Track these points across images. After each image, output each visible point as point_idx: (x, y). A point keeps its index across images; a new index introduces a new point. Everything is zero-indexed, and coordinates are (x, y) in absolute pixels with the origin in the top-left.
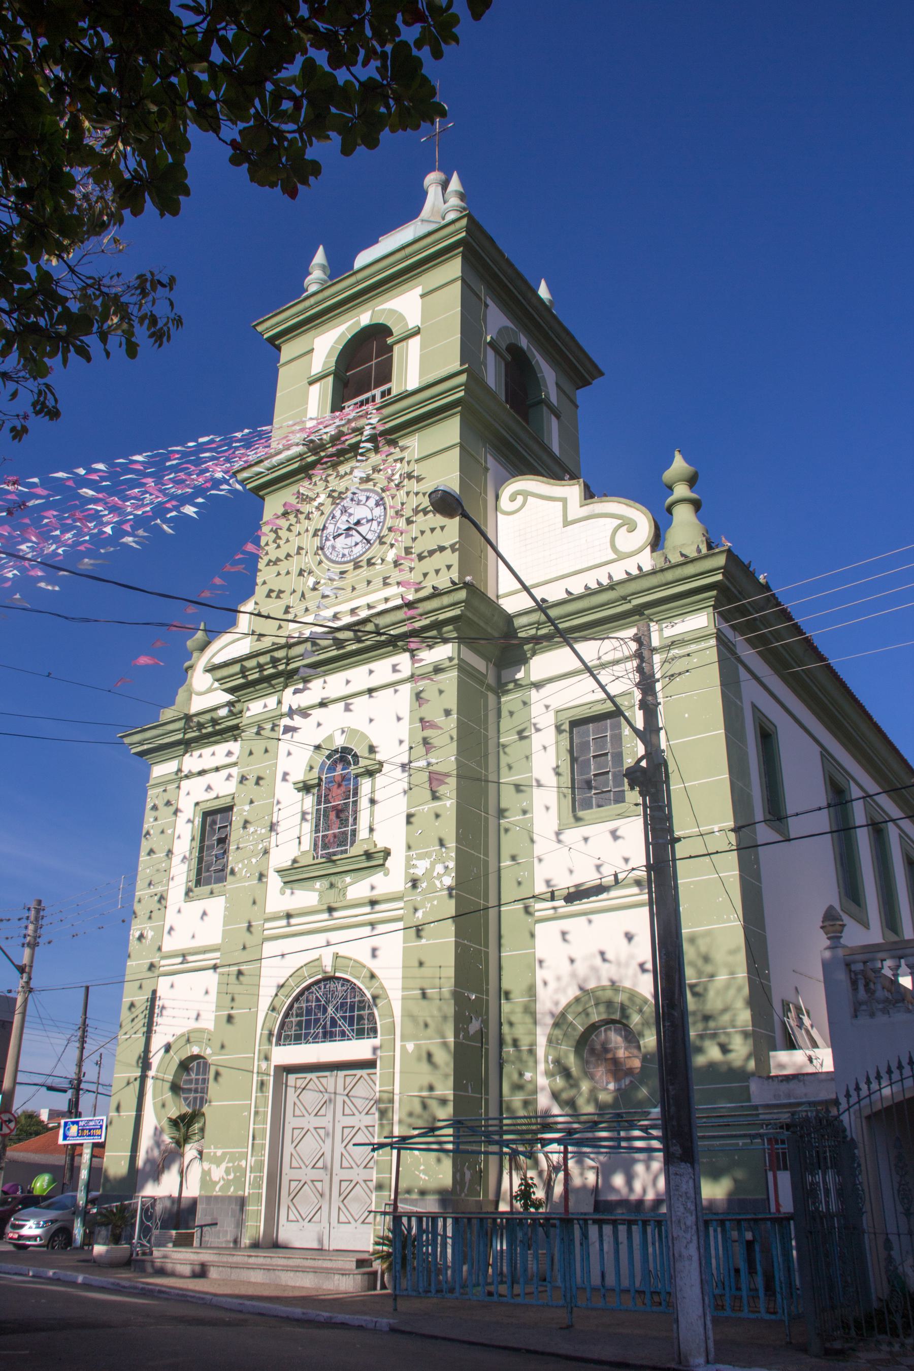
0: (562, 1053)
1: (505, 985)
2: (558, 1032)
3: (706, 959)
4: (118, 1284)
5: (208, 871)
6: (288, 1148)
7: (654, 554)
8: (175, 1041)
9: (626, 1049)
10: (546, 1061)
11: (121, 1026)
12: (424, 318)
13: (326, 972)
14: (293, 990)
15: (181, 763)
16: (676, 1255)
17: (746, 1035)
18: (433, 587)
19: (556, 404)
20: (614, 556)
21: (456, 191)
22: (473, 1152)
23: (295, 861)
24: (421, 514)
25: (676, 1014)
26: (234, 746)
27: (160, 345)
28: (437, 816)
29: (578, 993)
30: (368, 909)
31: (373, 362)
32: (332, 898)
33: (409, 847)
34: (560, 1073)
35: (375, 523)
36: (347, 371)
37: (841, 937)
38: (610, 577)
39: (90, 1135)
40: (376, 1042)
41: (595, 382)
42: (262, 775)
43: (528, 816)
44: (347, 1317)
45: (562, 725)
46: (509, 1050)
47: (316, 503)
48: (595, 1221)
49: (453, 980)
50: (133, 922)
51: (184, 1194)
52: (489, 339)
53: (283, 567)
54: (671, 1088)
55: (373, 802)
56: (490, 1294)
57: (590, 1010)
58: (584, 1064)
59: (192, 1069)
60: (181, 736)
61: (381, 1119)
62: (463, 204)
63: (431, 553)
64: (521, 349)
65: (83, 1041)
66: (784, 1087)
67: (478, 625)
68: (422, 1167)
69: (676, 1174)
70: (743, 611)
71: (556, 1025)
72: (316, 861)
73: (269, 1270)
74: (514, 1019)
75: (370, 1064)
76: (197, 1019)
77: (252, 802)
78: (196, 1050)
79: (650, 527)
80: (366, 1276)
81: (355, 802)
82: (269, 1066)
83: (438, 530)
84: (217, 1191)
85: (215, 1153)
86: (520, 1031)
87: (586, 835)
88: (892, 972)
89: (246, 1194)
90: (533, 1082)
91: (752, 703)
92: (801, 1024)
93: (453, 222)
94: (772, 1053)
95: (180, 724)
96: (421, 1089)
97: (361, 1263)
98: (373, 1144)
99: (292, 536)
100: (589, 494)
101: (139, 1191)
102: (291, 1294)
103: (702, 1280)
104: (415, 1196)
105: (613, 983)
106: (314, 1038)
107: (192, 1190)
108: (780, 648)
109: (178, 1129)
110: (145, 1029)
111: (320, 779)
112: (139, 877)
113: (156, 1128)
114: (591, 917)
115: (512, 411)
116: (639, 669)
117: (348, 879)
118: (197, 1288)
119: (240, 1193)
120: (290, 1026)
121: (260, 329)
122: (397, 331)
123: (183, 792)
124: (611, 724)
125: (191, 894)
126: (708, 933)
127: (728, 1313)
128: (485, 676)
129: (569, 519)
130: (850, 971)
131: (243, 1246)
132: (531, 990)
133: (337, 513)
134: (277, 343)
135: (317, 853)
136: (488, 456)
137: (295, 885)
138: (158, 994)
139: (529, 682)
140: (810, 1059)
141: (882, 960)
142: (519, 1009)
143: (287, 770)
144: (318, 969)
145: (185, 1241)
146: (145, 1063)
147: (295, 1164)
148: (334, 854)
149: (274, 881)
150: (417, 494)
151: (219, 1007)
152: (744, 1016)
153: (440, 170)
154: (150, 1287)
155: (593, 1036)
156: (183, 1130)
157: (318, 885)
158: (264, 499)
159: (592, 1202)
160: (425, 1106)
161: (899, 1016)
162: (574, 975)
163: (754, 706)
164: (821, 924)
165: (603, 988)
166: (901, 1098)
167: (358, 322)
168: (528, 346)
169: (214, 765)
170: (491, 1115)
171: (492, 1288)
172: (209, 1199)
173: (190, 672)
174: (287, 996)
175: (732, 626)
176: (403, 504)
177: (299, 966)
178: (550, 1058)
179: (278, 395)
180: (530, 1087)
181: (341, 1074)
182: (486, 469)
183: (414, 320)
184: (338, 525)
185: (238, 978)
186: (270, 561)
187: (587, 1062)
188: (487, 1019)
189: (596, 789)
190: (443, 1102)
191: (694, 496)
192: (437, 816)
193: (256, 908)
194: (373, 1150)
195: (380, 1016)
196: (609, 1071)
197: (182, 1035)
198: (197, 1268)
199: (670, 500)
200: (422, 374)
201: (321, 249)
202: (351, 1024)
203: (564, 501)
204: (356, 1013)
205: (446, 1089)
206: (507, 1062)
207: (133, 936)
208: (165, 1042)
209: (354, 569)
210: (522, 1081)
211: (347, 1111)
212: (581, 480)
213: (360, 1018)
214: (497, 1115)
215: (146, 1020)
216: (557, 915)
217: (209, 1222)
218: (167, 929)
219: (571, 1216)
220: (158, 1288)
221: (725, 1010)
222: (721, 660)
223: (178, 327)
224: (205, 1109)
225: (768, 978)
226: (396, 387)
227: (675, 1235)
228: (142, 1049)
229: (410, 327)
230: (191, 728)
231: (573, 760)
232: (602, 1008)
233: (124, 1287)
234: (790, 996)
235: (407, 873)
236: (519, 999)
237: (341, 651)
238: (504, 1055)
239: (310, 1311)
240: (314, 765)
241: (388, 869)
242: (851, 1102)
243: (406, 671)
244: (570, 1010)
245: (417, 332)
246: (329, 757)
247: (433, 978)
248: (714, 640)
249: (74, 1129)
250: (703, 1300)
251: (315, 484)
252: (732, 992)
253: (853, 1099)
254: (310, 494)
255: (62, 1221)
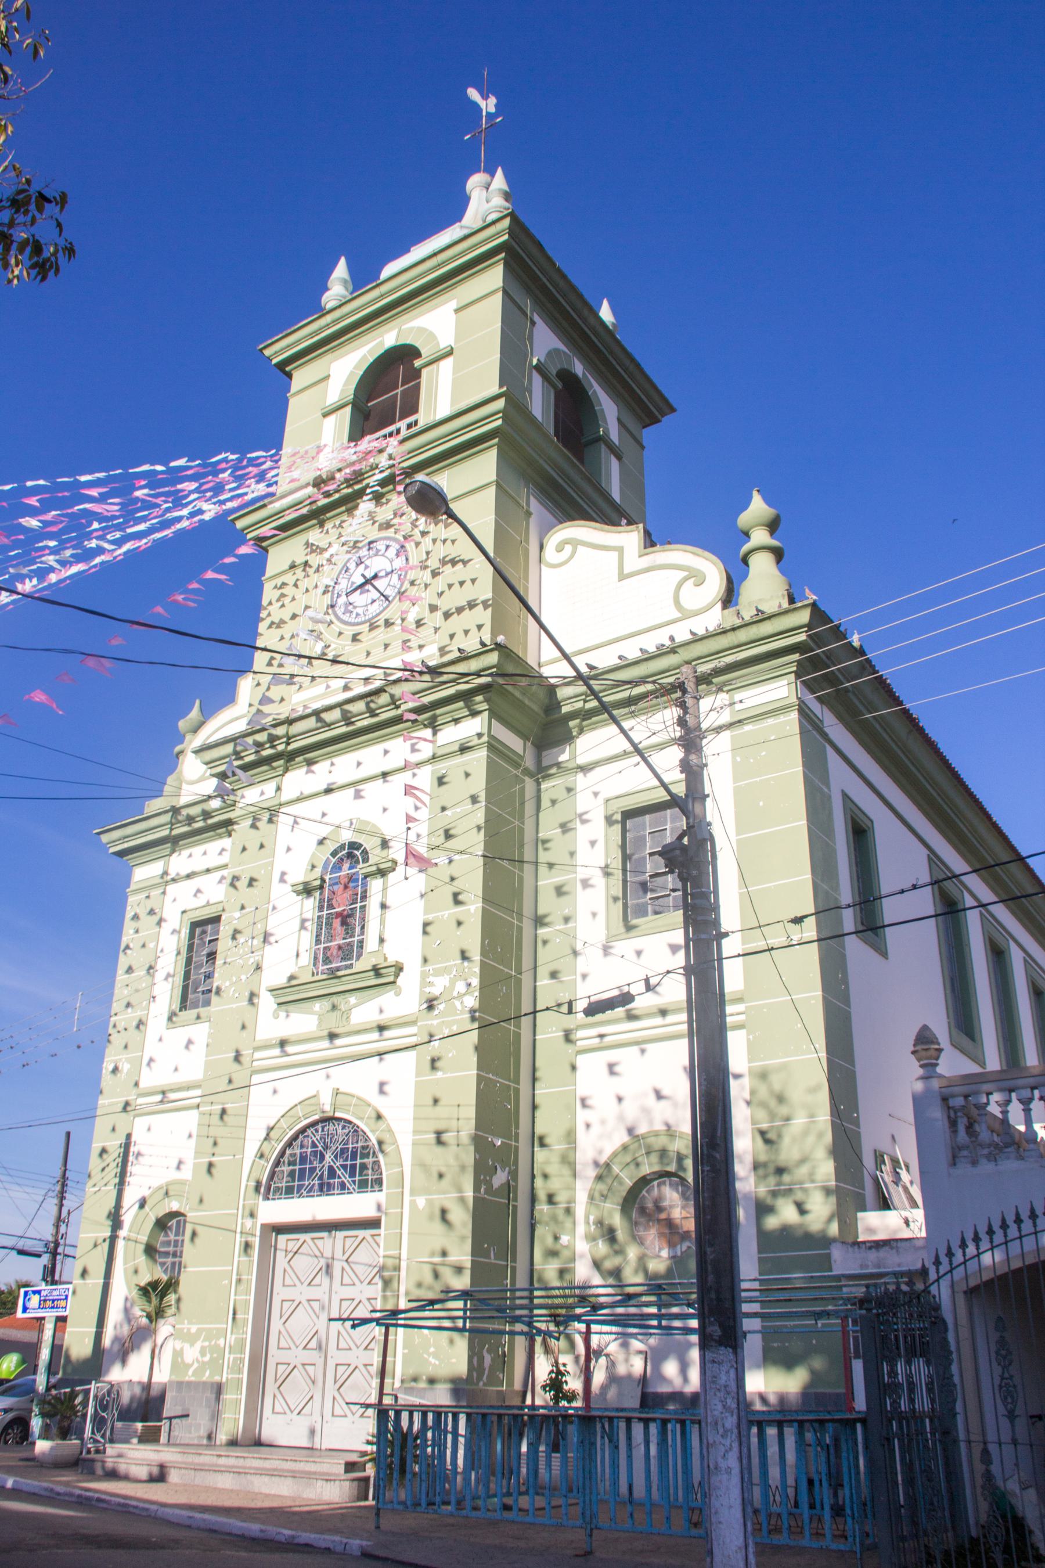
0: (605, 1214)
1: (539, 1130)
2: (601, 1187)
3: (781, 1099)
4: (52, 1490)
5: (195, 991)
6: (276, 1324)
7: (726, 611)
8: (151, 1195)
9: (683, 1207)
10: (587, 1222)
11: (89, 1176)
12: (458, 338)
13: (323, 1112)
14: (284, 1133)
15: (167, 865)
16: (711, 1466)
17: (827, 1191)
18: (459, 650)
19: (617, 443)
20: (678, 615)
21: (500, 190)
22: (494, 1332)
23: (292, 978)
24: (450, 565)
25: (718, 1156)
26: (226, 842)
27: (44, 279)
28: (459, 923)
29: (625, 1138)
30: (375, 1035)
31: (399, 391)
32: (333, 1023)
33: (425, 960)
34: (603, 1236)
35: (395, 577)
36: (368, 401)
37: (937, 1065)
38: (672, 639)
39: (53, 1307)
40: (381, 1197)
41: (665, 419)
42: (255, 876)
43: (570, 925)
44: (313, 1536)
45: (613, 815)
46: (542, 1208)
47: (327, 555)
48: (640, 1419)
49: (473, 1122)
50: (107, 1051)
51: (154, 1379)
52: (535, 362)
53: (287, 630)
54: (709, 1250)
55: (384, 906)
56: (507, 1508)
57: (640, 1159)
58: (633, 1225)
59: (170, 1228)
60: (166, 833)
61: (384, 1290)
62: (507, 205)
63: (460, 610)
64: (575, 377)
65: (62, 1198)
66: (873, 1256)
67: (513, 695)
68: (432, 1350)
69: (714, 1362)
70: (830, 680)
71: (599, 1178)
72: (316, 978)
73: (239, 1473)
74: (551, 1170)
75: (373, 1224)
76: (178, 1168)
77: (243, 908)
78: (175, 1206)
79: (721, 579)
80: (356, 1483)
81: (363, 907)
82: (254, 1225)
83: (468, 583)
84: (190, 1376)
85: (189, 1329)
86: (555, 1184)
87: (639, 948)
88: (1000, 1109)
89: (224, 1380)
90: (569, 1247)
91: (843, 791)
92: (897, 1180)
93: (494, 223)
94: (860, 1215)
95: (166, 818)
96: (432, 1254)
97: (350, 1467)
98: (353, 1320)
99: (298, 593)
100: (650, 541)
101: (105, 1376)
102: (259, 1504)
103: (743, 1499)
104: (422, 1385)
105: (668, 1126)
106: (310, 1191)
107: (162, 1376)
108: (837, 673)
109: (149, 1301)
110: (117, 1180)
111: (323, 880)
112: (115, 998)
113: (127, 1299)
114: (644, 1046)
115: (560, 445)
116: (682, 722)
117: (352, 999)
118: (146, 1496)
119: (217, 1378)
120: (280, 1176)
121: (267, 352)
122: (426, 352)
123: (168, 898)
124: (671, 815)
125: (174, 1019)
126: (784, 1067)
127: (783, 1539)
128: (522, 758)
129: (626, 571)
130: (949, 1108)
131: (218, 1443)
132: (570, 1136)
133: (352, 565)
134: (288, 369)
135: (317, 968)
136: (532, 498)
137: (291, 1007)
138: (133, 1139)
139: (575, 765)
140: (907, 1222)
141: (989, 1094)
142: (555, 1158)
143: (285, 870)
144: (314, 1108)
145: (150, 1437)
146: (115, 1219)
147: (283, 1344)
148: (338, 969)
149: (267, 1002)
150: (445, 541)
151: (198, 1153)
152: (826, 1169)
153: (485, 171)
154: (88, 1494)
155: (644, 1192)
156: (155, 1301)
157: (317, 1006)
158: (267, 551)
159: (639, 1394)
160: (436, 1275)
161: (1009, 1165)
162: (621, 1118)
163: (845, 796)
164: (912, 1048)
165: (656, 1134)
166: (1006, 1270)
167: (382, 343)
168: (584, 374)
169: (204, 867)
170: (518, 1285)
171: (508, 1501)
172: (180, 1385)
173: (181, 758)
174: (279, 1140)
175: (818, 698)
176: (428, 553)
177: (292, 1105)
178: (592, 1218)
179: (288, 429)
180: (565, 1253)
181: (340, 1235)
182: (529, 514)
183: (446, 339)
184: (352, 579)
185: (221, 1118)
186: (273, 623)
187: (636, 1224)
188: (516, 1170)
189: (652, 891)
190: (459, 1270)
191: (775, 543)
192: (459, 923)
193: (244, 1033)
194: (354, 1326)
195: (386, 1164)
196: (661, 1235)
197: (160, 1188)
198: (155, 1471)
199: (746, 548)
200: (453, 402)
201: (343, 261)
202: (352, 1174)
203: (620, 550)
204: (358, 1161)
205: (462, 1255)
206: (540, 1223)
207: (107, 1069)
208: (139, 1196)
209: (370, 630)
210: (558, 1247)
211: (346, 1280)
212: (641, 526)
213: (364, 1167)
214: (526, 1285)
215: (119, 1170)
216: (602, 1045)
217: (180, 1413)
218: (145, 1060)
219: (594, 1413)
220: (97, 1495)
221: (803, 1161)
222: (803, 732)
223: (70, 258)
224: (183, 1278)
225: (856, 1122)
226: (423, 418)
227: (711, 1441)
228: (113, 1204)
229: (442, 347)
230: (180, 822)
231: (626, 857)
232: (654, 1158)
233: (59, 1494)
234: (885, 1146)
235: (422, 992)
236: (557, 1145)
237: (351, 728)
238: (536, 1213)
239: (269, 1528)
240: (316, 864)
241: (399, 987)
242: (941, 1272)
243: (426, 750)
244: (616, 1160)
245: (450, 353)
246: (334, 854)
247: (449, 1119)
248: (796, 712)
249: (35, 1300)
250: (745, 1525)
251: (327, 532)
252: (811, 1139)
253: (944, 1267)
254: (323, 544)
255: (17, 1410)
